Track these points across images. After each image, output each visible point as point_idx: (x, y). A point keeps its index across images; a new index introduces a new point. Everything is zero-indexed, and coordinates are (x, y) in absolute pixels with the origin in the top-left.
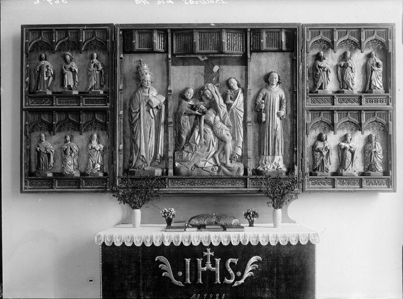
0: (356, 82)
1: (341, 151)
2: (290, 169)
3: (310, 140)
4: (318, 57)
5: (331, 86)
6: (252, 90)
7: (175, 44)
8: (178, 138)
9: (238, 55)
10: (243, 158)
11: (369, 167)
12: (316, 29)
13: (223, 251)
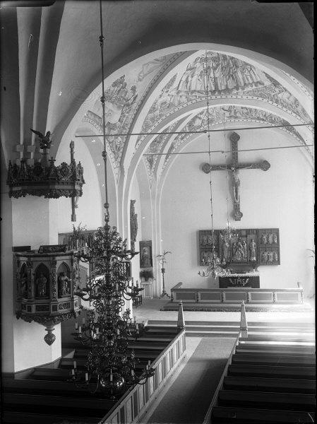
0: (271, 240)
3: (261, 254)
5: (266, 242)
6: (248, 243)
13: (242, 278)
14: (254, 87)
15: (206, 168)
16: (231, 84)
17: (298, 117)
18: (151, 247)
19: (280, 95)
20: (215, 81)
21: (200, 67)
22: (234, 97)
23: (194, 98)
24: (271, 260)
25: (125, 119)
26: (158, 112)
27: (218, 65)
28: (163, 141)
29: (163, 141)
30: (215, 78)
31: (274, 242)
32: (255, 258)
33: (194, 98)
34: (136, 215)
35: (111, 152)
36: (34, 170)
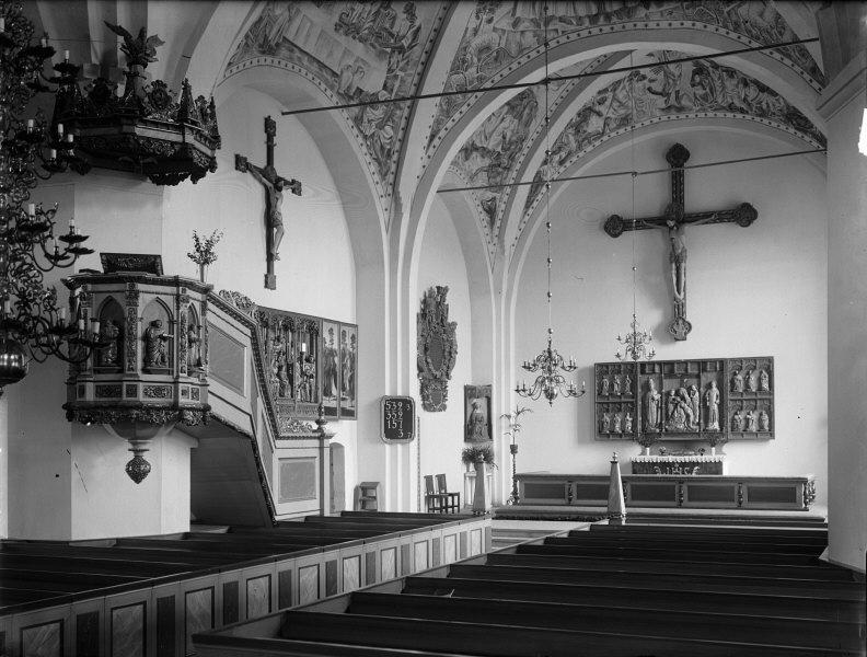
1: (747, 420)
2: (722, 429)
4: (735, 374)
7: (666, 369)
8: (667, 414)
9: (515, 289)
10: (699, 424)
11: (761, 427)
12: (733, 360)
13: (683, 465)
15: (616, 226)
17: (787, 61)
18: (489, 400)
22: (640, 25)
24: (754, 427)
25: (397, 84)
26: (473, 70)
28: (518, 166)
29: (518, 166)
31: (760, 388)
32: (716, 425)
34: (454, 324)
35: (368, 158)
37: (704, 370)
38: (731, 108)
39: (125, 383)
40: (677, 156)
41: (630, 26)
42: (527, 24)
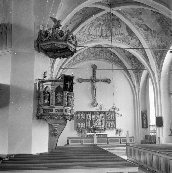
14: (120, 36)
16: (109, 34)
19: (131, 41)
20: (101, 31)
21: (96, 23)
23: (91, 38)
27: (104, 24)
30: (102, 30)
33: (91, 38)
36: (59, 34)
37: (101, 114)
38: (107, 59)
39: (65, 109)
40: (94, 67)
41: (107, 39)
42: (86, 35)
